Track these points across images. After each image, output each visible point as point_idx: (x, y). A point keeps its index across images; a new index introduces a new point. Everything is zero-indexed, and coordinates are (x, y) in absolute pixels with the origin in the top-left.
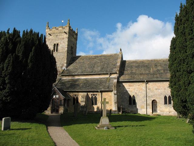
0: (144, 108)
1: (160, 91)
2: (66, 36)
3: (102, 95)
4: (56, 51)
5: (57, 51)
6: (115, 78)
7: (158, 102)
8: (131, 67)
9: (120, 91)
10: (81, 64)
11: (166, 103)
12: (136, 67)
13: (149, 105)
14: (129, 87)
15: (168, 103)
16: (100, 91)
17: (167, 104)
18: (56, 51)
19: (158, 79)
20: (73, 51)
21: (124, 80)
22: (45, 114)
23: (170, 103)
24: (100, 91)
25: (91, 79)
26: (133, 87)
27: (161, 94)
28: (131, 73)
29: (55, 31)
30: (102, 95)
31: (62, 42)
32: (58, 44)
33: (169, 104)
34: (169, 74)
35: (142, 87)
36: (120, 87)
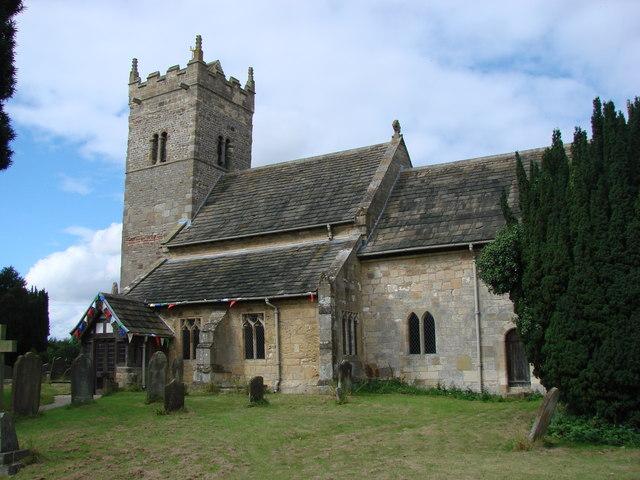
0: (470, 368)
2: (188, 100)
3: (279, 314)
4: (159, 160)
5: (163, 160)
6: (347, 245)
8: (432, 192)
10: (246, 199)
12: (451, 191)
13: (492, 351)
14: (407, 279)
15: (255, 356)
16: (271, 301)
17: (252, 357)
18: (159, 160)
20: (227, 153)
24: (271, 301)
25: (262, 254)
26: (424, 277)
28: (423, 217)
29: (154, 87)
30: (279, 314)
31: (177, 125)
32: (165, 134)
35: (459, 274)
36: (373, 281)
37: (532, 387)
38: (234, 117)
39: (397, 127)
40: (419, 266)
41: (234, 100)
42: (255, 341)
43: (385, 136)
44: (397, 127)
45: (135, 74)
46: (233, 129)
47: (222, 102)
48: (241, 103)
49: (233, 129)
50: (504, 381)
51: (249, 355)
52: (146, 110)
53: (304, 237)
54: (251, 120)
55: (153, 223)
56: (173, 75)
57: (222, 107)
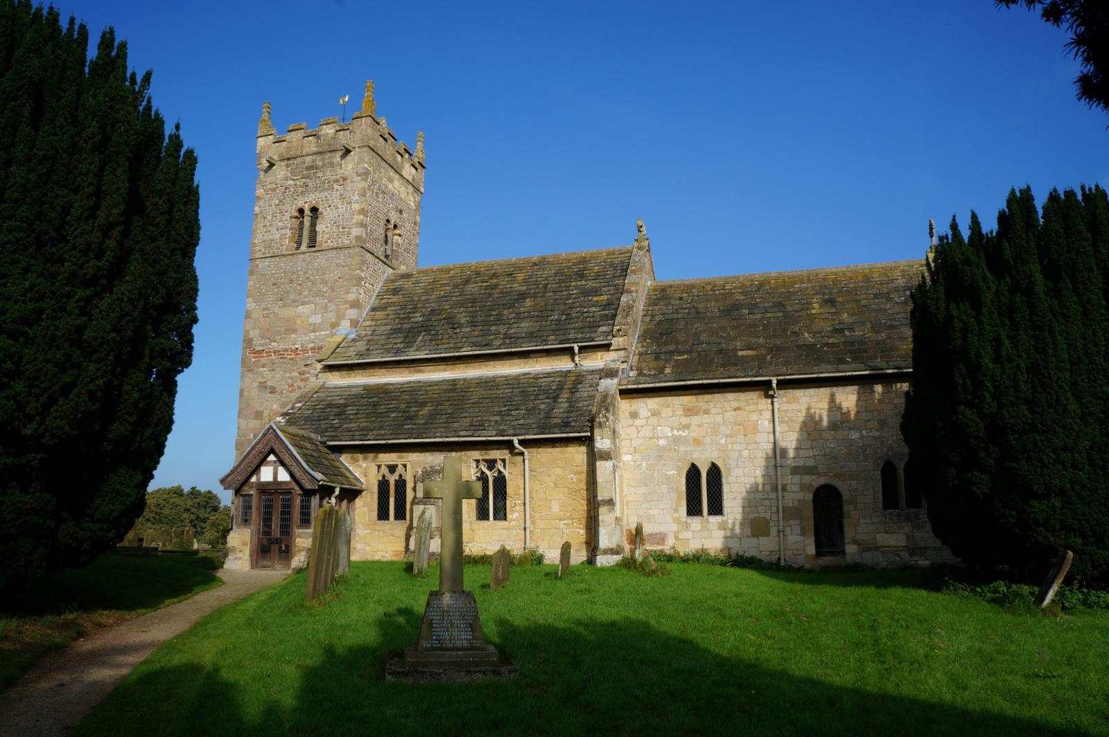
7: (846, 495)
14: (685, 420)
15: (903, 501)
17: (896, 506)
19: (842, 367)
21: (530, 491)
23: (913, 502)
24: (521, 442)
26: (706, 419)
34: (956, 326)
36: (638, 422)
37: (848, 558)
41: (404, 173)
42: (392, 501)
46: (401, 212)
47: (392, 173)
49: (401, 212)
50: (811, 550)
51: (482, 514)
55: (294, 331)
57: (391, 180)
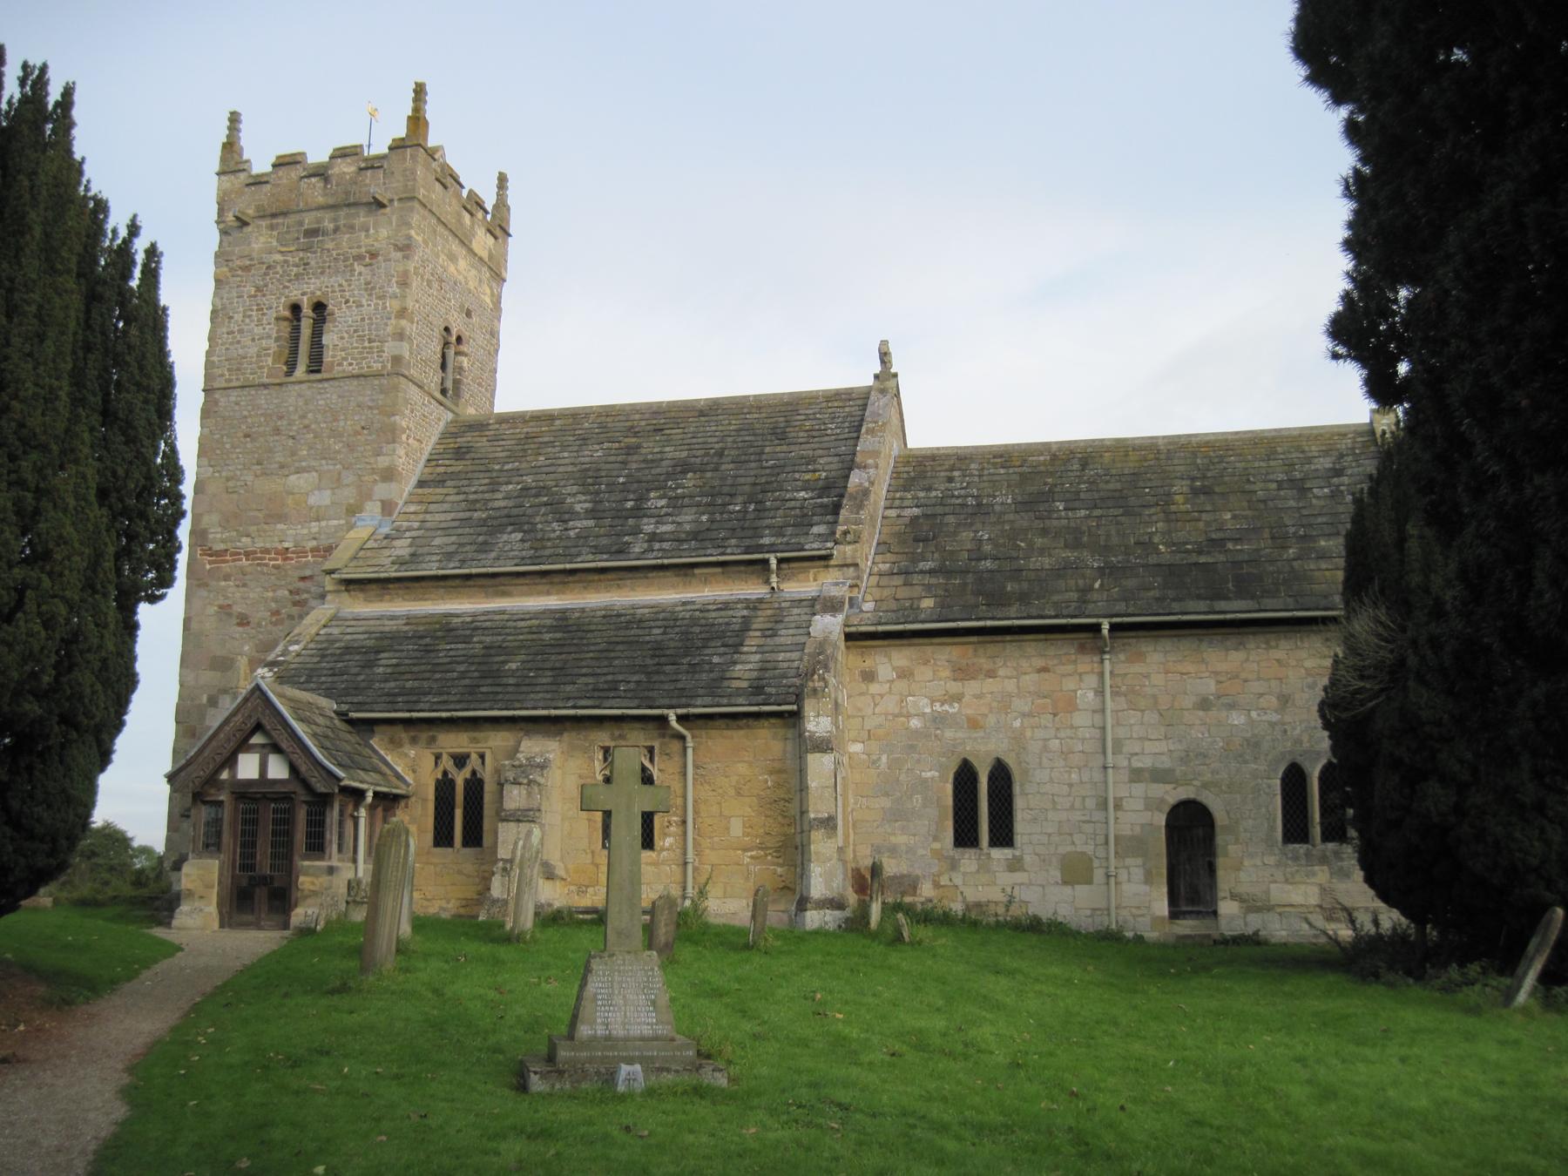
1: (1237, 719)
7: (1220, 817)
9: (869, 724)
11: (1295, 830)
14: (954, 687)
15: (1316, 831)
18: (300, 371)
19: (1222, 605)
20: (460, 369)
22: (1357, 892)
25: (611, 617)
26: (989, 685)
27: (1254, 744)
32: (319, 307)
33: (466, 844)
35: (1070, 684)
36: (874, 688)
38: (472, 285)
39: (884, 356)
40: (983, 662)
41: (475, 246)
43: (860, 375)
44: (884, 356)
45: (231, 147)
46: (469, 314)
47: (455, 247)
48: (485, 255)
49: (469, 314)
50: (1162, 907)
52: (260, 240)
53: (706, 581)
54: (500, 297)
55: (282, 518)
56: (347, 168)
57: (453, 258)
